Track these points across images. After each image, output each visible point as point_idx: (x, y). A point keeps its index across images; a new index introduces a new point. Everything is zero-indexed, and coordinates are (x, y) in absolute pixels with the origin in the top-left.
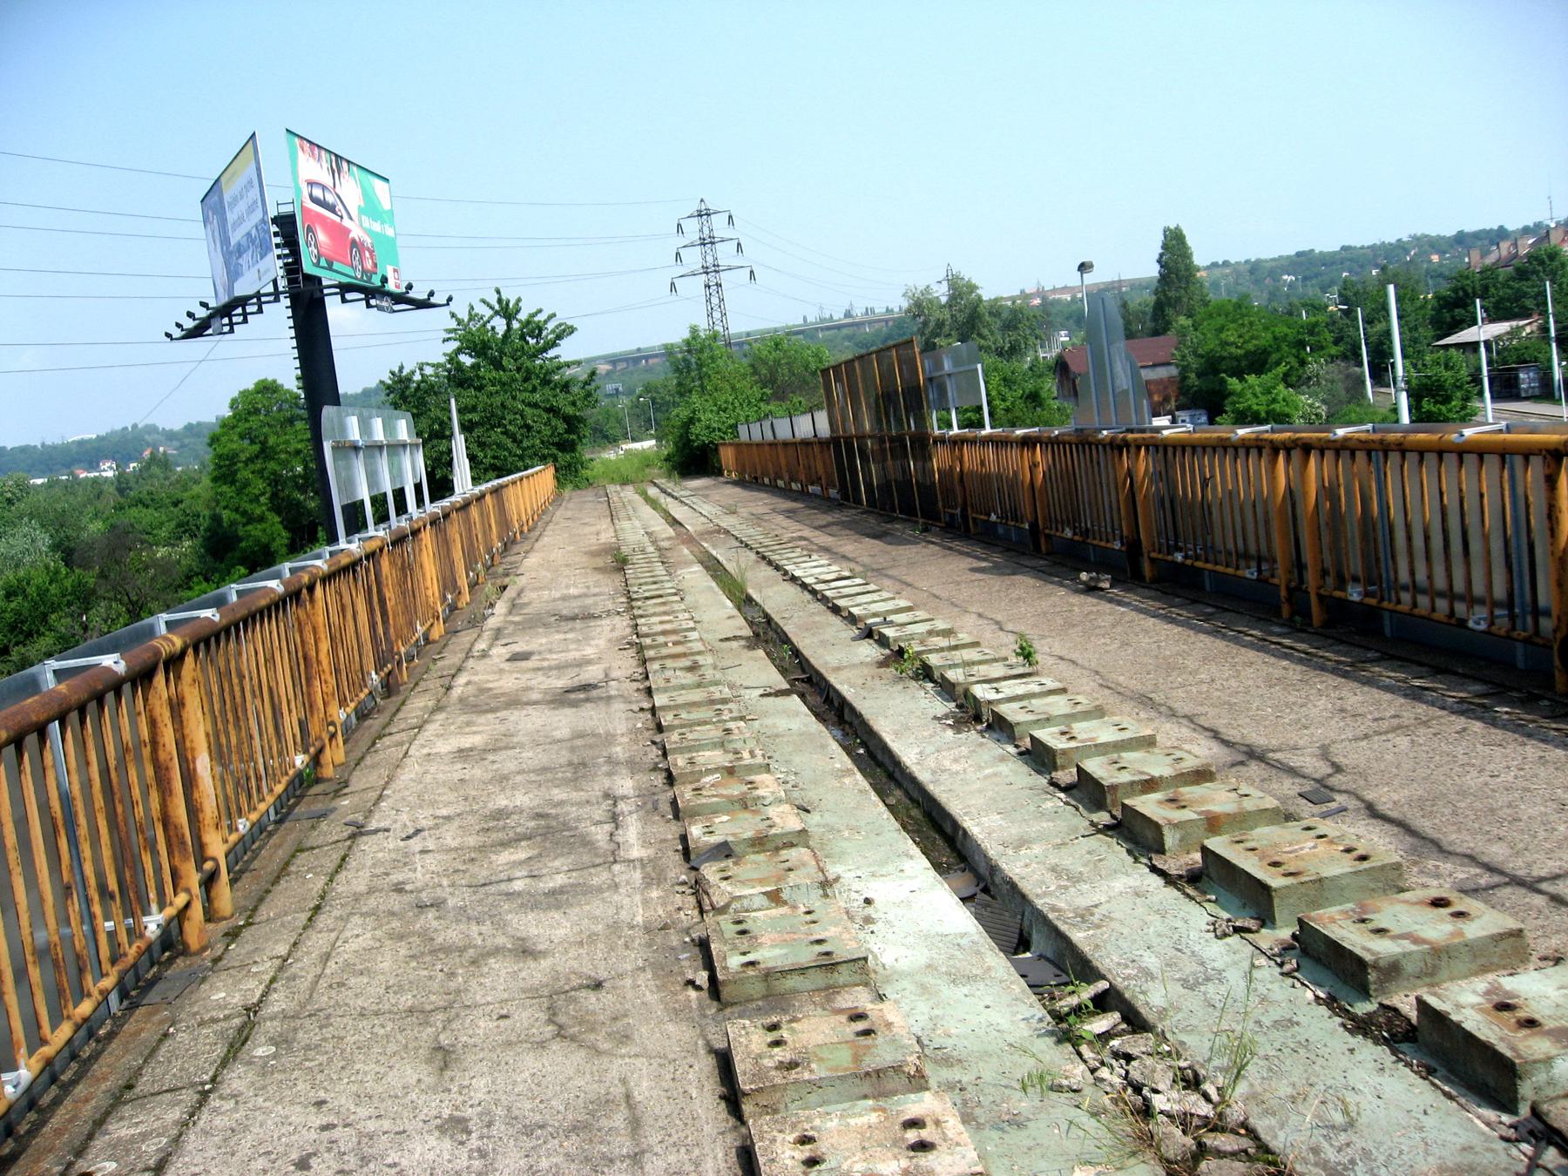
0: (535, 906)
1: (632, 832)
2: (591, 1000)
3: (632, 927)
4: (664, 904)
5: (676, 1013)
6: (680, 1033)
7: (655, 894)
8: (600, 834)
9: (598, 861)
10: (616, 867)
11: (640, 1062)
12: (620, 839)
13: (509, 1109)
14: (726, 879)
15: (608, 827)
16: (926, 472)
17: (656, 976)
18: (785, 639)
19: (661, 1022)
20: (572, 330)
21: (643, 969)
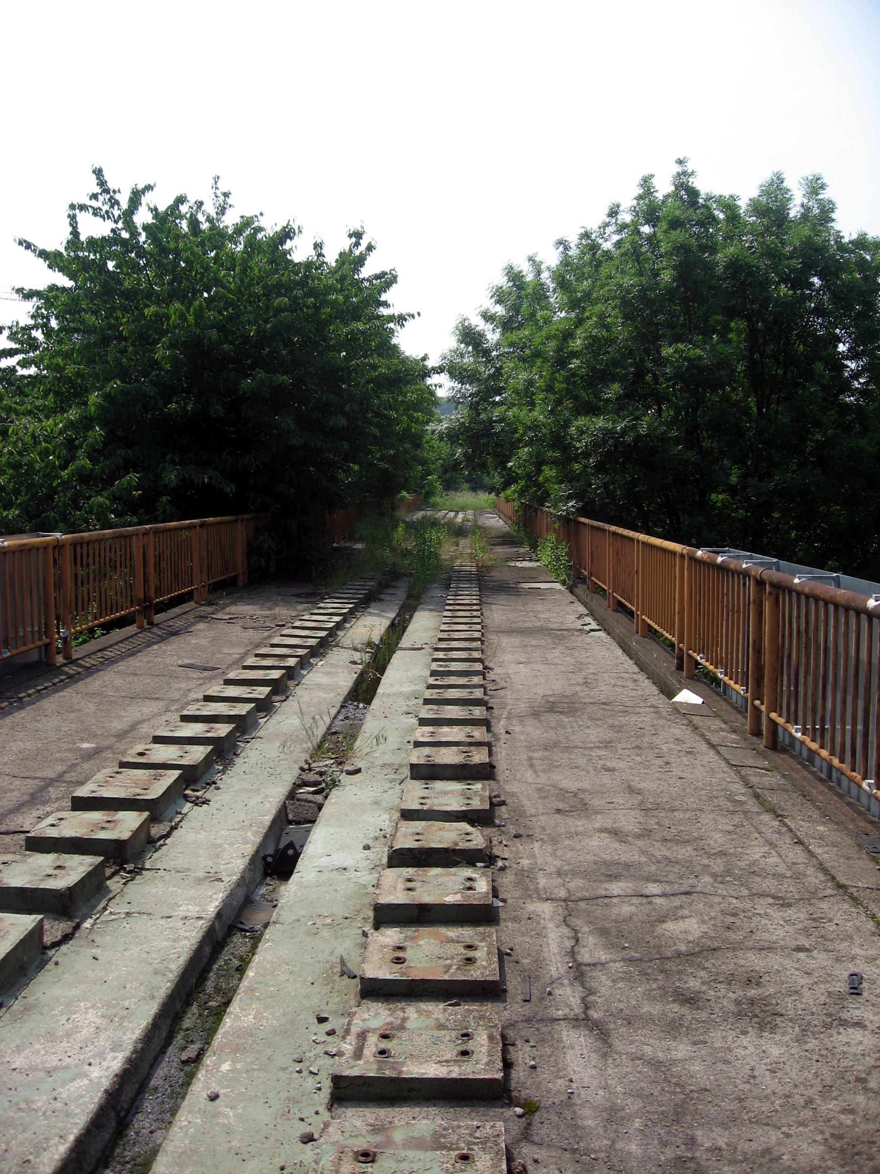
0: (627, 866)
1: (555, 941)
2: (561, 806)
3: (541, 840)
4: (517, 852)
5: (513, 795)
6: (513, 787)
7: (525, 862)
8: (592, 950)
9: (582, 904)
10: (562, 894)
11: (531, 781)
12: (565, 930)
13: (752, 1070)
14: (467, 834)
15: (585, 956)
16: (779, 295)
17: (524, 812)
18: (382, 670)
19: (521, 793)
20: (20, 291)
21: (532, 816)
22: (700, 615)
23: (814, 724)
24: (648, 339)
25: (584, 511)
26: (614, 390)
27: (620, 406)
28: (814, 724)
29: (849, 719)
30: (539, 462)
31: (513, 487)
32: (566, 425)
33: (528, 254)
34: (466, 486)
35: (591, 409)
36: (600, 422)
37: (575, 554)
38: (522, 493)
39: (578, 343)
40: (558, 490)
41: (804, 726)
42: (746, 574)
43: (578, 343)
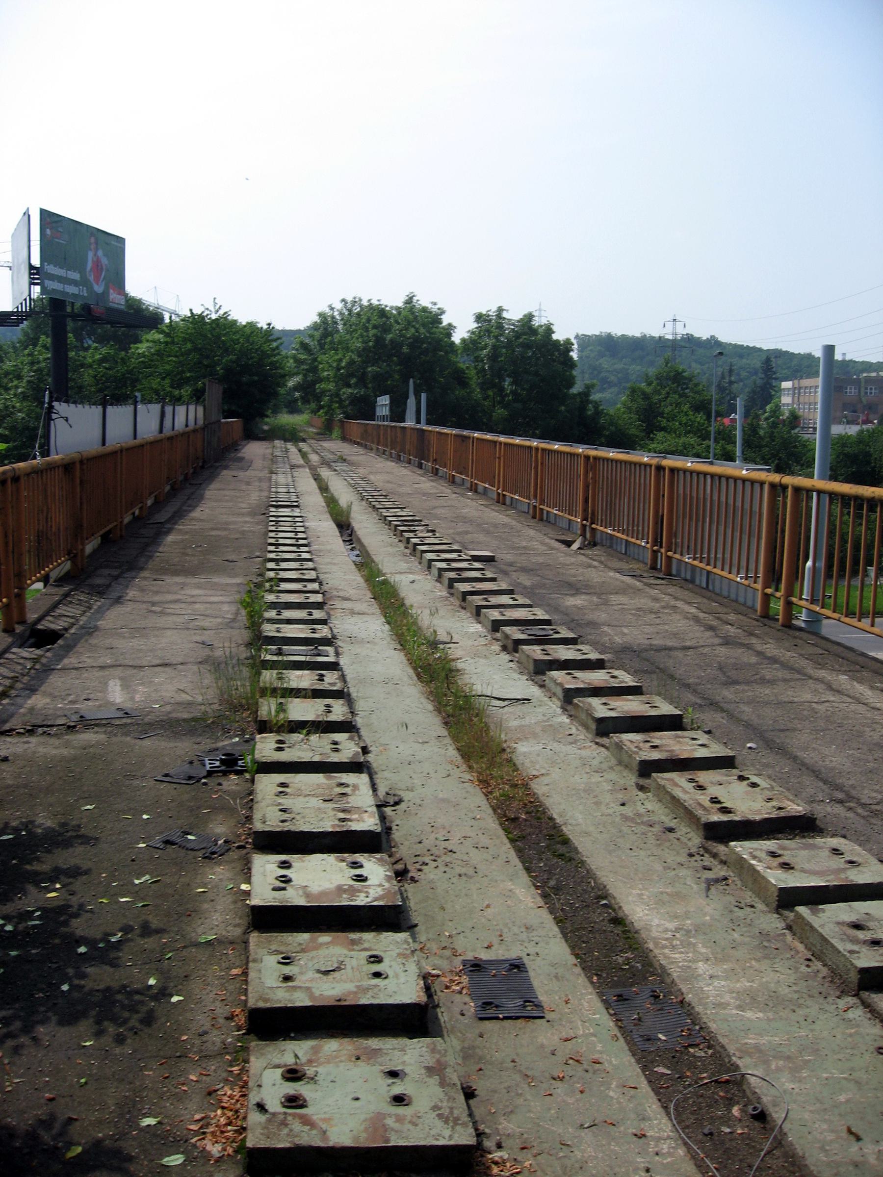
22: (620, 488)
23: (702, 554)
24: (366, 362)
25: (345, 418)
26: (353, 381)
27: (356, 385)
28: (702, 554)
29: (706, 550)
30: (331, 401)
31: (322, 411)
32: (339, 391)
33: (478, 311)
34: (285, 410)
35: (349, 386)
36: (350, 390)
37: (343, 432)
38: (326, 413)
39: (343, 364)
40: (338, 411)
41: (695, 553)
42: (646, 465)
43: (343, 364)
